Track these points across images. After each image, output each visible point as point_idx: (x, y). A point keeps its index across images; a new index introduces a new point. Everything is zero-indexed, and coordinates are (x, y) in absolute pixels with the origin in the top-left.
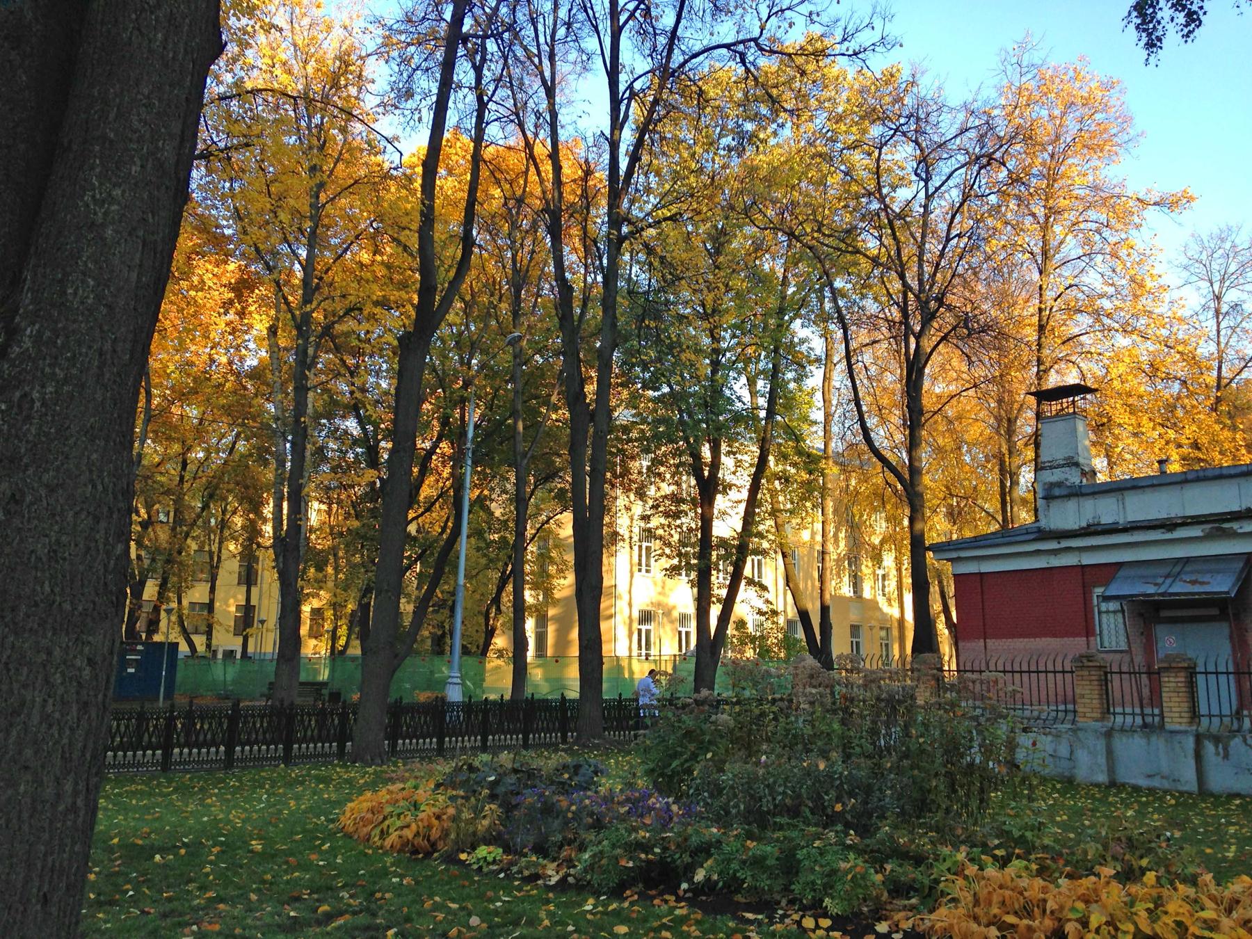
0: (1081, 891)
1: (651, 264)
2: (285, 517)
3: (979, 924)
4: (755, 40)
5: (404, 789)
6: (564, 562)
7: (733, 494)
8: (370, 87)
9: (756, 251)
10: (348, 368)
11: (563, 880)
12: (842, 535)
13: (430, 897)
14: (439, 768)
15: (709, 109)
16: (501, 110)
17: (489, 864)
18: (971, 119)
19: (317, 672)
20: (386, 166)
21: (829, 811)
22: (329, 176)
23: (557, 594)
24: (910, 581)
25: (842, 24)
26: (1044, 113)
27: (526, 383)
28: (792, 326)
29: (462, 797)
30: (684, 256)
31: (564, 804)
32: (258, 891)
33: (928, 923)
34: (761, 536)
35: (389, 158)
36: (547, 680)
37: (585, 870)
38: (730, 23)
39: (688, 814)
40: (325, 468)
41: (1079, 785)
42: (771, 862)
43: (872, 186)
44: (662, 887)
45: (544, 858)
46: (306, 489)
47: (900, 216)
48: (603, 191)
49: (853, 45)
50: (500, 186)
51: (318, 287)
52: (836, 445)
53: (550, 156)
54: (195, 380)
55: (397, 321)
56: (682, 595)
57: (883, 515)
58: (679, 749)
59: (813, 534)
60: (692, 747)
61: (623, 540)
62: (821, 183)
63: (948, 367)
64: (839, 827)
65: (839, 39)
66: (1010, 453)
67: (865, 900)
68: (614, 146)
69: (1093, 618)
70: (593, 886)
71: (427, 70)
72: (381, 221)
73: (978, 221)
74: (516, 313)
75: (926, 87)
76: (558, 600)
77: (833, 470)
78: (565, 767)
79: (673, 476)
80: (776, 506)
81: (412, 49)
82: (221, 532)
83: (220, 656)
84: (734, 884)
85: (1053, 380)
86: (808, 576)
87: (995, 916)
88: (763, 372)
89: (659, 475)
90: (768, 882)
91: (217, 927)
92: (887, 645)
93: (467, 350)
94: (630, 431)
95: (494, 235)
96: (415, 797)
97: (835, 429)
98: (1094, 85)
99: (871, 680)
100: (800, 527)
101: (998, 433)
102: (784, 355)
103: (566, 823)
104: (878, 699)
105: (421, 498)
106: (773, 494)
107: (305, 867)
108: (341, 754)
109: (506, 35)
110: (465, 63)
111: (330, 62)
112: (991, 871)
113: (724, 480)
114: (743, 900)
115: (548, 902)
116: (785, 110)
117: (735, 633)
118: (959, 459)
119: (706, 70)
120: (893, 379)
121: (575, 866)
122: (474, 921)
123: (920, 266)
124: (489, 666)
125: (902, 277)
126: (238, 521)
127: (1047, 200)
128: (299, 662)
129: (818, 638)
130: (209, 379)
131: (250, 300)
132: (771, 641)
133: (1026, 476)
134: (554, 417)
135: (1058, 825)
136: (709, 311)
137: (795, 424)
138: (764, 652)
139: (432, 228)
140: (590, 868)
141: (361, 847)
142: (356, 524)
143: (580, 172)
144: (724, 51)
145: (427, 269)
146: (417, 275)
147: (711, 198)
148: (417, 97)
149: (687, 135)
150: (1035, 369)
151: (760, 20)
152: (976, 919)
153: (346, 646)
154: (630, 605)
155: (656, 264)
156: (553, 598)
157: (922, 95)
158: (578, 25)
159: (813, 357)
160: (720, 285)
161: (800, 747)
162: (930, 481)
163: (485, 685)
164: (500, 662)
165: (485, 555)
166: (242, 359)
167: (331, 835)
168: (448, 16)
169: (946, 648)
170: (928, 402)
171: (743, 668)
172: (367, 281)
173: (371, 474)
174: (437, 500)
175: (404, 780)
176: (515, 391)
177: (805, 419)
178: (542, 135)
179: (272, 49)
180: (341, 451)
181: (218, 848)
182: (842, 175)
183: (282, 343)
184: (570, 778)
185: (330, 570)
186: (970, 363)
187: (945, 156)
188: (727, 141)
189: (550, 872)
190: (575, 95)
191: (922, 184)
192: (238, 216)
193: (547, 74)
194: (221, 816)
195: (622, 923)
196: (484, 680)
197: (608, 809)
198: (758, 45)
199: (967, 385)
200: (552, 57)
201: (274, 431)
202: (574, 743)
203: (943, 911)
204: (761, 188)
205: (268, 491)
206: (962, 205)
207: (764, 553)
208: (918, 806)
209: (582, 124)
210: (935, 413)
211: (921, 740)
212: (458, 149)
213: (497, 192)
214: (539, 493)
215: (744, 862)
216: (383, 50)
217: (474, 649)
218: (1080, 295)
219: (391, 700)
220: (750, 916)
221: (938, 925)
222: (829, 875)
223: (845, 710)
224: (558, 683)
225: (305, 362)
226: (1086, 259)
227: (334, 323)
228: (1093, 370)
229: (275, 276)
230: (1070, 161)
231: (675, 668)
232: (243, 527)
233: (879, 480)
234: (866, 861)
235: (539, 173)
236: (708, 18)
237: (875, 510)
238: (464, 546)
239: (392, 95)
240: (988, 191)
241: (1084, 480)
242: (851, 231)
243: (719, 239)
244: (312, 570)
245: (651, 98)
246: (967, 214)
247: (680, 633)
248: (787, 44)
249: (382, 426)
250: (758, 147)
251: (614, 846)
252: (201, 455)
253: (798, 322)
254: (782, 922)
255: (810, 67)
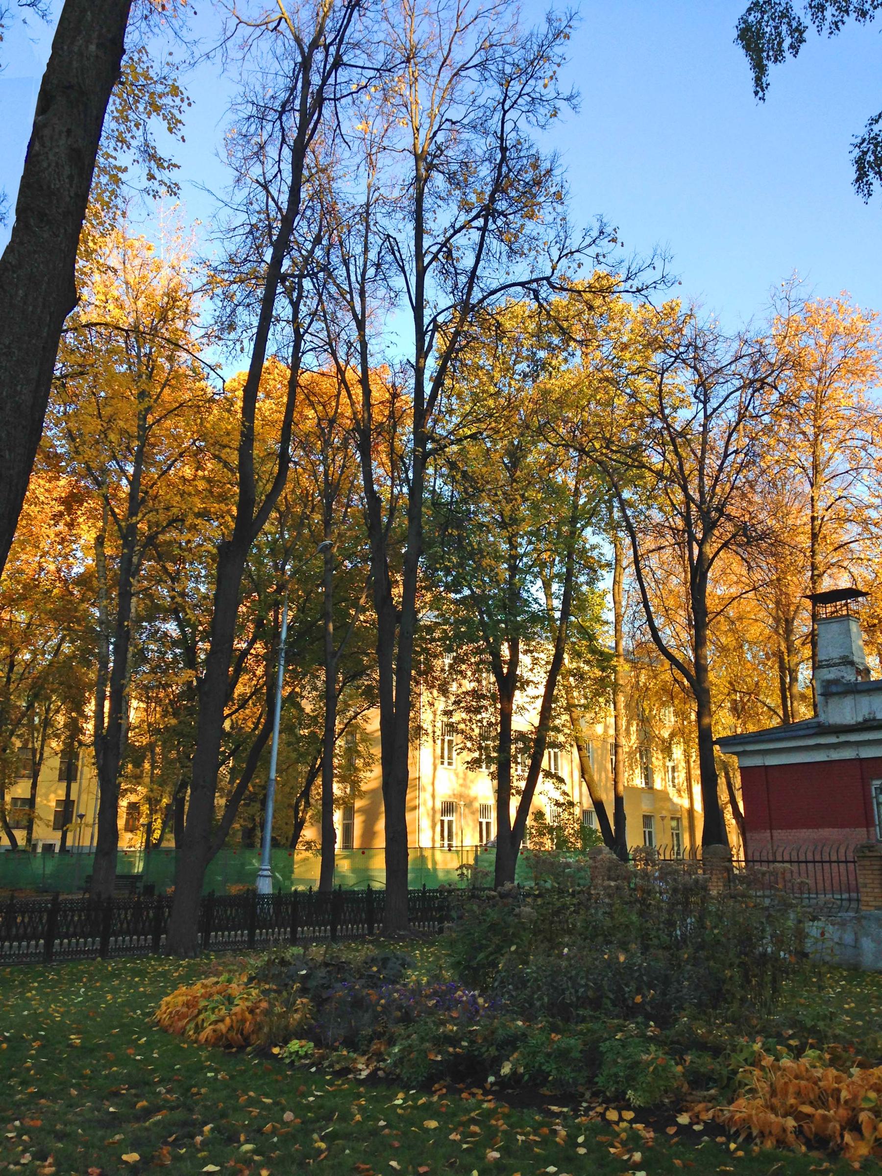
0: (874, 1080)
1: (453, 477)
2: (106, 715)
3: (777, 1115)
4: (547, 279)
5: (217, 983)
6: (371, 756)
7: (531, 690)
8: (196, 320)
9: (550, 465)
10: (169, 575)
11: (373, 1075)
12: (633, 728)
13: (245, 1092)
14: (252, 962)
15: (505, 340)
16: (315, 340)
17: (301, 1058)
18: (745, 348)
19: (132, 865)
20: (209, 390)
21: (630, 1002)
22: (156, 401)
23: (364, 787)
24: (699, 772)
25: (625, 265)
26: (811, 342)
27: (336, 587)
28: (584, 533)
29: (275, 991)
30: (484, 470)
31: (374, 998)
32: (77, 1086)
33: (727, 1114)
34: (557, 730)
35: (213, 384)
36: (354, 870)
37: (395, 1065)
38: (525, 264)
39: (493, 1007)
40: (146, 668)
41: (864, 972)
42: (576, 1054)
43: (655, 408)
44: (469, 1081)
45: (354, 1052)
46: (127, 689)
47: (682, 434)
48: (408, 411)
49: (636, 283)
50: (314, 408)
51: (143, 501)
52: (626, 643)
53: (360, 381)
54: (24, 588)
55: (215, 531)
56: (483, 787)
57: (672, 709)
58: (484, 942)
59: (606, 727)
60: (496, 940)
61: (427, 734)
62: (610, 403)
63: (728, 571)
64: (640, 1019)
65: (623, 277)
66: (789, 651)
67: (666, 1092)
68: (419, 372)
69: (873, 810)
70: (402, 1080)
71: (248, 305)
72: (204, 440)
73: (752, 439)
74: (327, 522)
75: (702, 319)
76: (365, 792)
77: (624, 667)
78: (374, 960)
79: (474, 674)
80: (571, 701)
81: (235, 286)
82: (45, 730)
83: (39, 850)
84: (539, 1077)
85: (826, 585)
86: (602, 768)
87: (792, 1106)
88: (557, 575)
89: (461, 672)
90: (572, 1075)
91: (39, 1123)
92: (678, 835)
93: (281, 557)
94: (434, 631)
95: (308, 453)
96: (229, 991)
97: (625, 628)
98: (855, 317)
99: (667, 871)
100: (594, 721)
101: (776, 632)
102: (576, 558)
103: (376, 1018)
104: (675, 890)
105: (235, 695)
106: (568, 689)
107: (123, 1061)
108: (155, 947)
109: (321, 275)
110: (283, 300)
111: (158, 298)
112: (786, 1062)
113: (522, 676)
114: (548, 1093)
115: (359, 1096)
116: (575, 340)
117: (534, 824)
118: (741, 657)
119: (503, 305)
120: (678, 582)
121: (384, 1060)
122: (288, 1116)
123: (701, 480)
124: (297, 857)
125: (685, 489)
126: (61, 720)
127: (815, 420)
128: (116, 857)
129: (613, 828)
130: (37, 586)
131: (79, 512)
132: (569, 831)
133: (805, 673)
134: (362, 618)
135: (847, 1012)
136: (507, 521)
137: (588, 624)
138: (562, 842)
139: (251, 447)
140: (400, 1061)
141: (177, 1041)
142: (173, 722)
143: (387, 395)
144: (519, 288)
145: (247, 483)
146: (236, 489)
147: (508, 419)
148: (239, 330)
149: (486, 361)
150: (810, 573)
151: (552, 261)
152: (773, 1109)
153: (160, 840)
154: (433, 796)
155: (458, 477)
156: (359, 791)
157: (700, 326)
158: (387, 266)
159: (603, 562)
160: (518, 497)
161: (600, 939)
162: (717, 678)
163: (293, 876)
164: (309, 854)
165: (295, 750)
166: (70, 567)
167: (146, 1030)
168: (268, 257)
169: (734, 838)
170: (711, 604)
171: (544, 861)
172: (190, 494)
173: (188, 675)
174: (250, 697)
175: (218, 974)
176: (326, 594)
177: (598, 619)
178: (353, 362)
179: (106, 286)
180: (161, 652)
181: (39, 1043)
182: (627, 397)
183: (108, 552)
184: (379, 971)
185: (147, 765)
186: (750, 568)
187: (722, 380)
188: (523, 367)
189: (360, 1066)
190: (383, 327)
191: (701, 406)
192: (70, 436)
193: (358, 309)
194: (41, 1010)
195: (431, 1118)
196: (292, 872)
197: (417, 1003)
198: (550, 283)
199: (747, 588)
200: (362, 294)
201: (98, 634)
202: (380, 935)
203: (742, 1102)
204: (553, 409)
205: (90, 690)
206: (738, 424)
207: (561, 746)
208: (715, 996)
209: (390, 353)
210: (718, 614)
211: (716, 931)
212: (276, 374)
213: (311, 413)
214: (347, 690)
215: (549, 1055)
216: (207, 287)
217: (284, 841)
218: (848, 506)
219: (206, 890)
220: (555, 1108)
221: (738, 1116)
222: (631, 1067)
223: (643, 902)
224: (364, 874)
225: (129, 569)
226: (854, 473)
227: (157, 533)
228: (863, 575)
229: (104, 491)
230: (836, 385)
231: (476, 858)
232: (65, 726)
233: (667, 677)
234: (666, 1053)
235: (350, 396)
236: (504, 259)
237: (663, 704)
238: (276, 740)
239: (216, 328)
240: (761, 413)
241: (859, 678)
242: (637, 448)
243: (516, 455)
244: (130, 766)
245: (452, 330)
246: (742, 433)
247: (481, 823)
248: (576, 281)
249: (200, 628)
250: (551, 373)
251: (422, 1040)
252: (28, 657)
253: (589, 530)
254: (586, 1114)
255: (598, 302)
